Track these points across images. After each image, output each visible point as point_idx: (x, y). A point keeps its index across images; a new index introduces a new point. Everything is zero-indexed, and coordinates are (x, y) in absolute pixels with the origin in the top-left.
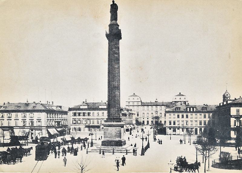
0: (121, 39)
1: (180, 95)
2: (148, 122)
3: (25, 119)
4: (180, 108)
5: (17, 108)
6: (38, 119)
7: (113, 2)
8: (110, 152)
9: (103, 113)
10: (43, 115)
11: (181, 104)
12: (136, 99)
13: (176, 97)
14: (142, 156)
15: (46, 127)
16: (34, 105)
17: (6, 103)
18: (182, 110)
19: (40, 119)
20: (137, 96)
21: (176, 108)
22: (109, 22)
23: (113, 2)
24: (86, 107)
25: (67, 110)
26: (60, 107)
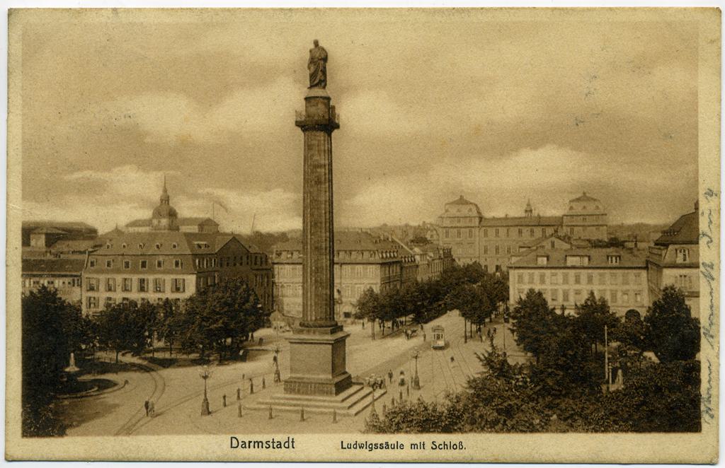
7: (316, 43)
23: (316, 43)
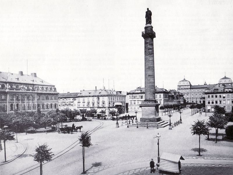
0: (155, 37)
1: (225, 78)
2: (12, 105)
3: (99, 101)
4: (218, 89)
5: (88, 95)
6: (103, 101)
7: (148, 9)
8: (145, 127)
9: (160, 96)
10: (106, 99)
11: (219, 86)
12: (186, 83)
13: (222, 80)
14: (83, 127)
15: (108, 107)
16: (100, 91)
17: (82, 90)
18: (220, 91)
19: (104, 101)
20: (187, 81)
21: (214, 89)
22: (145, 26)
23: (148, 9)
24: (140, 92)
25: (126, 94)
26: (120, 92)
